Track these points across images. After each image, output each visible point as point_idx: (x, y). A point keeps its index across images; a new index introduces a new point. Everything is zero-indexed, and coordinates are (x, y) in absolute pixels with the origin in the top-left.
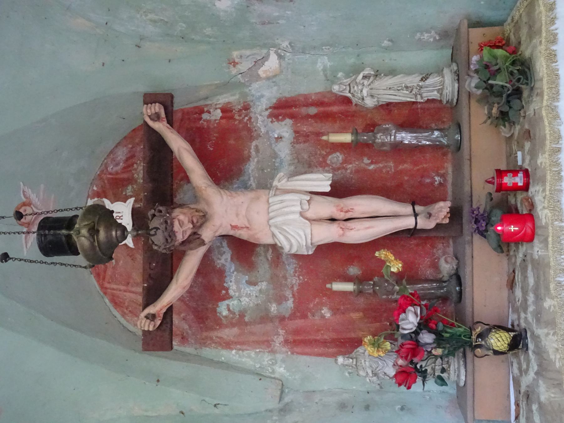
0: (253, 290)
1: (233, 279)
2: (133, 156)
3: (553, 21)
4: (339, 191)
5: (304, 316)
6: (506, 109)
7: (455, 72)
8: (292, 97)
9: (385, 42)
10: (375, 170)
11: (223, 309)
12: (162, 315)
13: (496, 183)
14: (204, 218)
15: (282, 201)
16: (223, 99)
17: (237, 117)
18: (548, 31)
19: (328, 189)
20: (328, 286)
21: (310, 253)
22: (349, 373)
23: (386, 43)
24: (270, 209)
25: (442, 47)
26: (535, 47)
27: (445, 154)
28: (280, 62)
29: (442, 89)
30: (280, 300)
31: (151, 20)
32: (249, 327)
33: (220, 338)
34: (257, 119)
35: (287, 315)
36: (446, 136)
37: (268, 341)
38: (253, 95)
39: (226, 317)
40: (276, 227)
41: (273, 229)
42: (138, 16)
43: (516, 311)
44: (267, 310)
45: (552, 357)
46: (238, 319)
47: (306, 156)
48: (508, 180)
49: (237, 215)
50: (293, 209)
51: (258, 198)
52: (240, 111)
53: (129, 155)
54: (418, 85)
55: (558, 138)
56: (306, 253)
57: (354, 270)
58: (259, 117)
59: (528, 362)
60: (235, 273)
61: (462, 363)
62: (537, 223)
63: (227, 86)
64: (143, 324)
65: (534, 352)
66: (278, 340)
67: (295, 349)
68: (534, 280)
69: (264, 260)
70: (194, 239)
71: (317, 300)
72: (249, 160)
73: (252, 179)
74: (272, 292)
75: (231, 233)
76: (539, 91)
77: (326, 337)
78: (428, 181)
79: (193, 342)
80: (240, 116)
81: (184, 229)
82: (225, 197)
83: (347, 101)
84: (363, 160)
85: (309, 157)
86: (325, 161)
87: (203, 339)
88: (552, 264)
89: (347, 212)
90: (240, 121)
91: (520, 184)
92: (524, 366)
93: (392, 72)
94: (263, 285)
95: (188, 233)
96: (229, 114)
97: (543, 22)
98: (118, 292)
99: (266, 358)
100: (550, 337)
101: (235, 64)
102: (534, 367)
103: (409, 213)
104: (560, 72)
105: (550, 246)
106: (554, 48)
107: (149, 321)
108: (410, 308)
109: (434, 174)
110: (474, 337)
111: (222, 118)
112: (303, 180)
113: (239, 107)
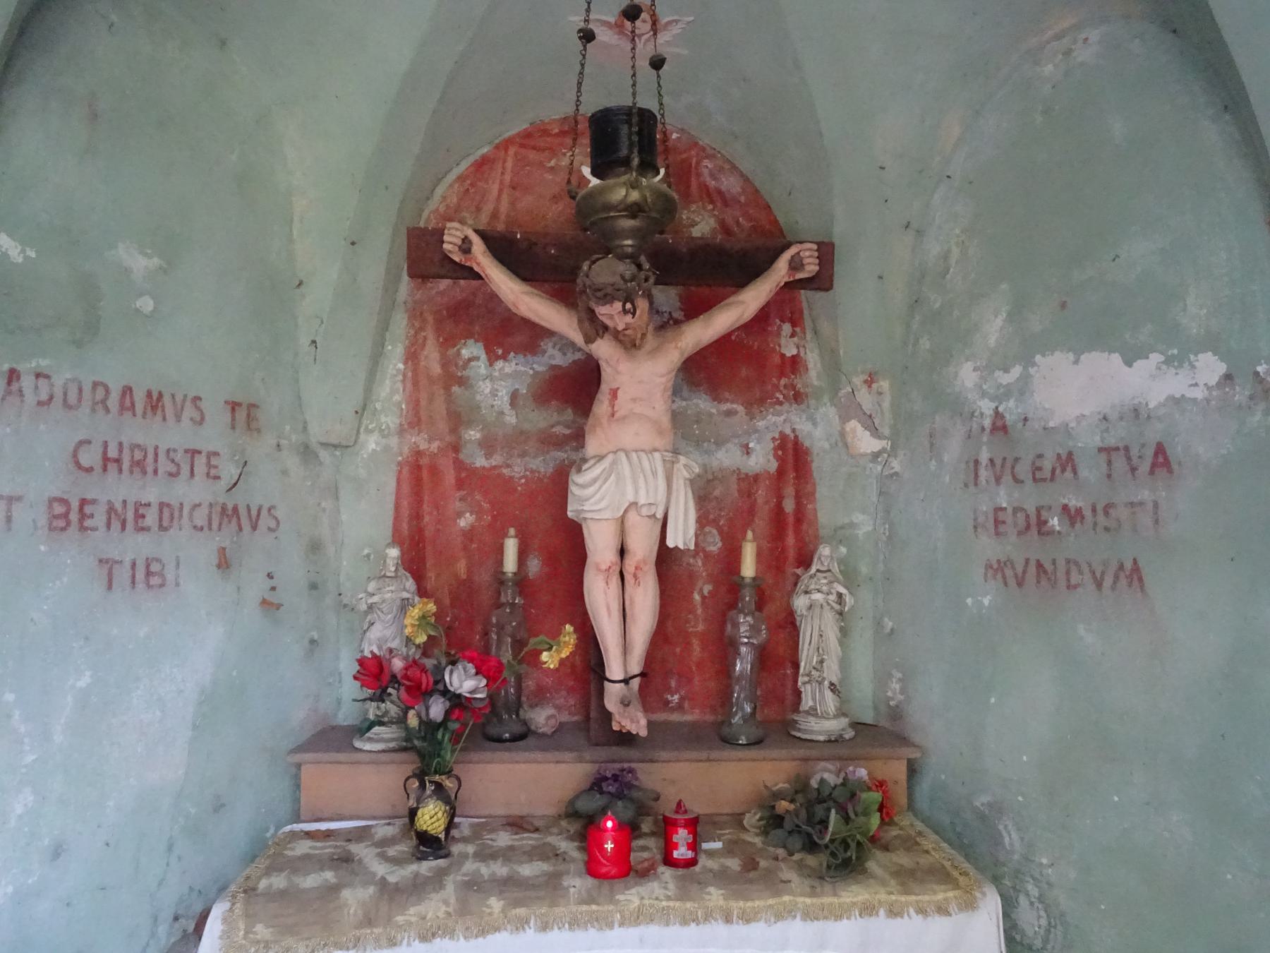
0: (503, 400)
2: (726, 203)
3: (922, 911)
4: (665, 558)
5: (460, 484)
6: (788, 825)
7: (841, 736)
10: (689, 598)
11: (471, 349)
13: (678, 817)
14: (629, 344)
15: (654, 474)
16: (812, 359)
17: (783, 381)
18: (908, 904)
20: (512, 531)
21: (570, 514)
22: (368, 556)
23: (889, 624)
24: (643, 455)
25: (876, 708)
26: (884, 883)
27: (713, 710)
29: (816, 715)
30: (488, 445)
31: (949, 251)
32: (442, 391)
33: (424, 345)
34: (779, 414)
35: (461, 456)
36: (745, 721)
39: (458, 354)
40: (614, 463)
41: (610, 457)
42: (957, 231)
44: (470, 424)
45: (412, 910)
46: (453, 377)
47: (717, 493)
48: (682, 836)
49: (634, 400)
50: (642, 492)
51: (660, 432)
52: (794, 387)
54: (824, 679)
55: (747, 918)
56: (569, 508)
57: (535, 566)
58: (782, 418)
59: (397, 861)
60: (531, 372)
61: (392, 745)
62: (618, 884)
63: (834, 367)
65: (417, 875)
66: (421, 441)
67: (406, 470)
68: (529, 878)
70: (595, 328)
71: (486, 506)
72: (714, 400)
73: (684, 403)
75: (604, 387)
76: (818, 890)
77: (427, 519)
78: (673, 684)
79: (418, 296)
80: (785, 386)
81: (616, 317)
82: (663, 380)
83: (805, 561)
84: (709, 583)
85: (716, 498)
86: (709, 523)
87: (421, 314)
88: (557, 910)
89: (635, 576)
90: (776, 387)
91: (676, 854)
92: (392, 852)
93: (844, 632)
94: (511, 419)
96: (788, 370)
97: (920, 898)
98: (500, 171)
99: (390, 420)
100: (444, 908)
101: (869, 383)
102: (396, 875)
103: (629, 669)
104: (845, 921)
105: (585, 908)
106: (882, 912)
107: (460, 243)
108: (484, 682)
109: (683, 693)
110: (437, 778)
111: (783, 356)
112: (686, 503)
113: (799, 386)
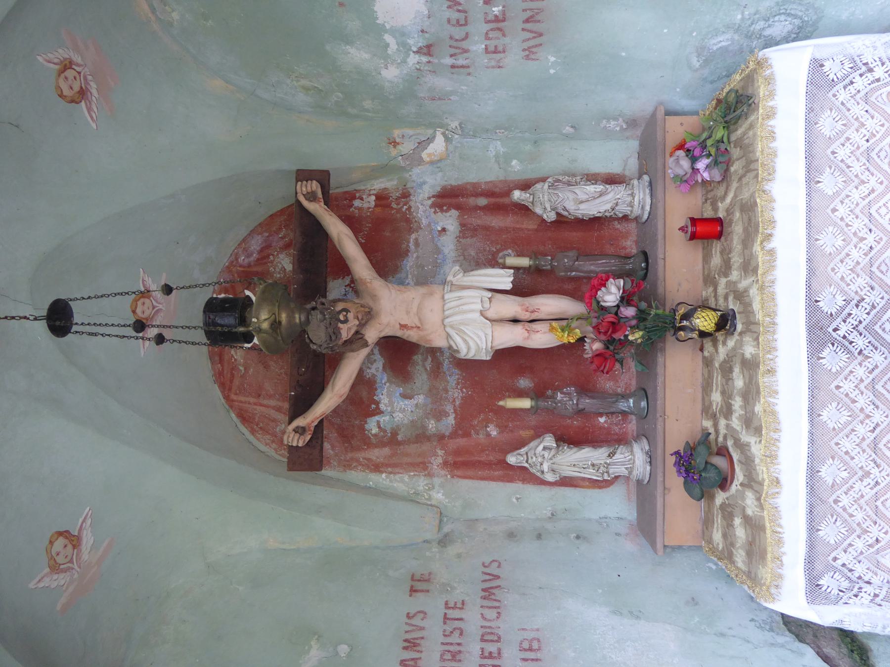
1: (385, 392)
8: (459, 185)
9: (567, 128)
11: (372, 426)
12: (312, 429)
14: (368, 316)
15: (460, 298)
17: (394, 205)
19: (509, 286)
21: (488, 358)
23: (568, 130)
24: (446, 307)
28: (446, 145)
30: (439, 415)
31: (303, 87)
32: (402, 447)
33: (369, 460)
37: (424, 463)
38: (414, 181)
39: (375, 435)
40: (452, 327)
41: (449, 330)
42: (289, 81)
43: (714, 418)
44: (424, 427)
46: (391, 439)
47: (473, 253)
49: (408, 313)
50: (473, 307)
52: (398, 198)
53: (264, 245)
57: (524, 383)
58: (421, 207)
60: (388, 384)
64: (290, 439)
69: (422, 369)
70: (357, 340)
73: (410, 276)
74: (430, 406)
75: (399, 333)
77: (491, 458)
79: (335, 464)
80: (398, 204)
94: (420, 399)
95: (353, 331)
96: (383, 202)
98: (247, 405)
99: (421, 483)
101: (395, 144)
111: (376, 206)
112: (480, 275)
